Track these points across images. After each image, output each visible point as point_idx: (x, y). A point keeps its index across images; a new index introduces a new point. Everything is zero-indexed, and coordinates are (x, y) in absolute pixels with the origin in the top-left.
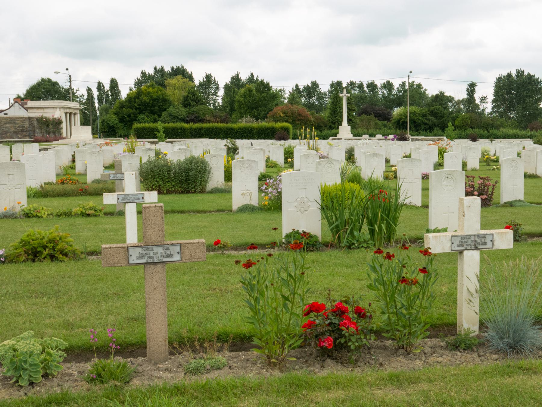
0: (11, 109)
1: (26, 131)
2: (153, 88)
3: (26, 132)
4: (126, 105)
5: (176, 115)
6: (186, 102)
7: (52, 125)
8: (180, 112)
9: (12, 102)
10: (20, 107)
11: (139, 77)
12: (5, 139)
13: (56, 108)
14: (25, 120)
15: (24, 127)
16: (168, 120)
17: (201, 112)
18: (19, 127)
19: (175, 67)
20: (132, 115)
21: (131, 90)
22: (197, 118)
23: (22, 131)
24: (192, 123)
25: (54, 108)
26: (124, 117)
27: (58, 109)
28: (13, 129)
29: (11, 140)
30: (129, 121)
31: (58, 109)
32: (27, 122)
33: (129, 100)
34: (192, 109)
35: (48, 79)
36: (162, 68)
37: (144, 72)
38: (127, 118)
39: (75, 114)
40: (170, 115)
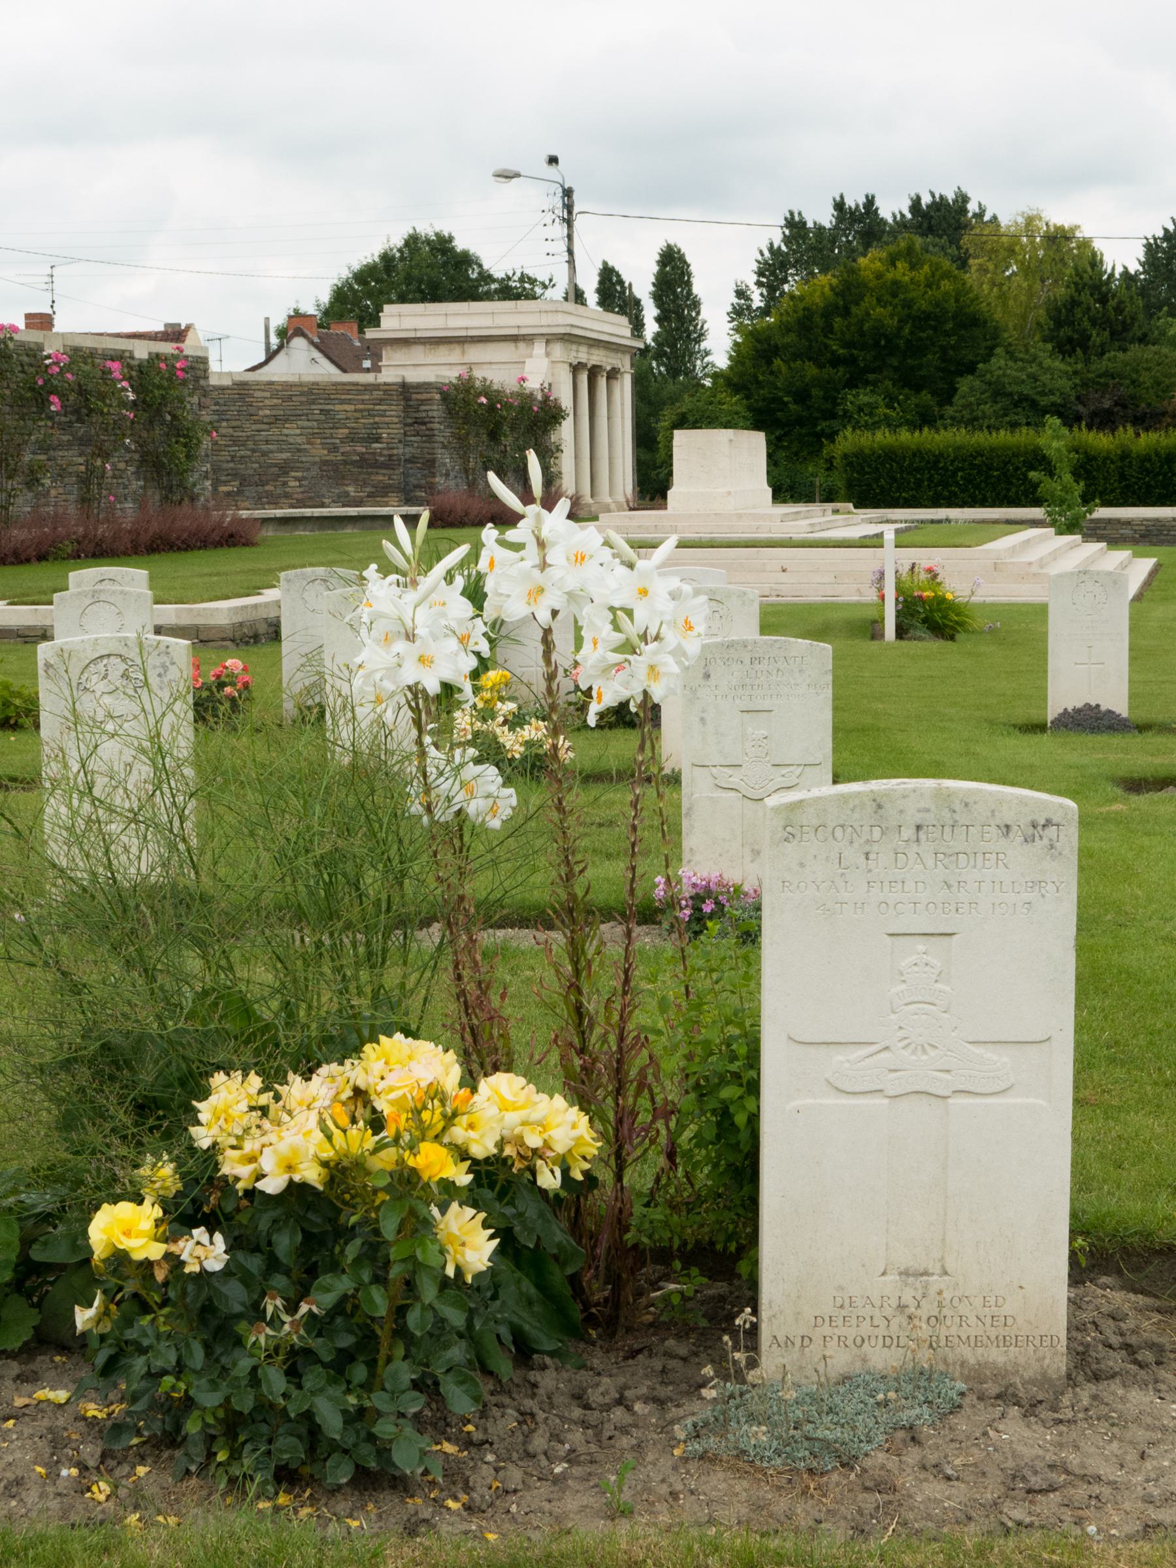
0: (272, 364)
1: (390, 463)
2: (913, 267)
3: (384, 466)
4: (786, 347)
5: (1026, 390)
6: (1065, 332)
7: (512, 429)
8: (1045, 378)
9: (275, 341)
10: (317, 354)
11: (778, 242)
12: (276, 505)
13: (528, 339)
14: (381, 402)
15: (378, 439)
16: (984, 417)
17: (1145, 378)
18: (352, 438)
19: (926, 200)
20: (815, 392)
21: (741, 294)
22: (1125, 407)
23: (367, 463)
24: (1131, 431)
25: (514, 339)
26: (776, 400)
27: (539, 348)
28: (319, 452)
29: (308, 512)
30: (800, 422)
31: (539, 348)
32: (393, 412)
33: (799, 322)
34: (1101, 365)
35: (437, 234)
36: (870, 201)
37: (797, 218)
38: (792, 407)
39: (613, 375)
40: (997, 392)
